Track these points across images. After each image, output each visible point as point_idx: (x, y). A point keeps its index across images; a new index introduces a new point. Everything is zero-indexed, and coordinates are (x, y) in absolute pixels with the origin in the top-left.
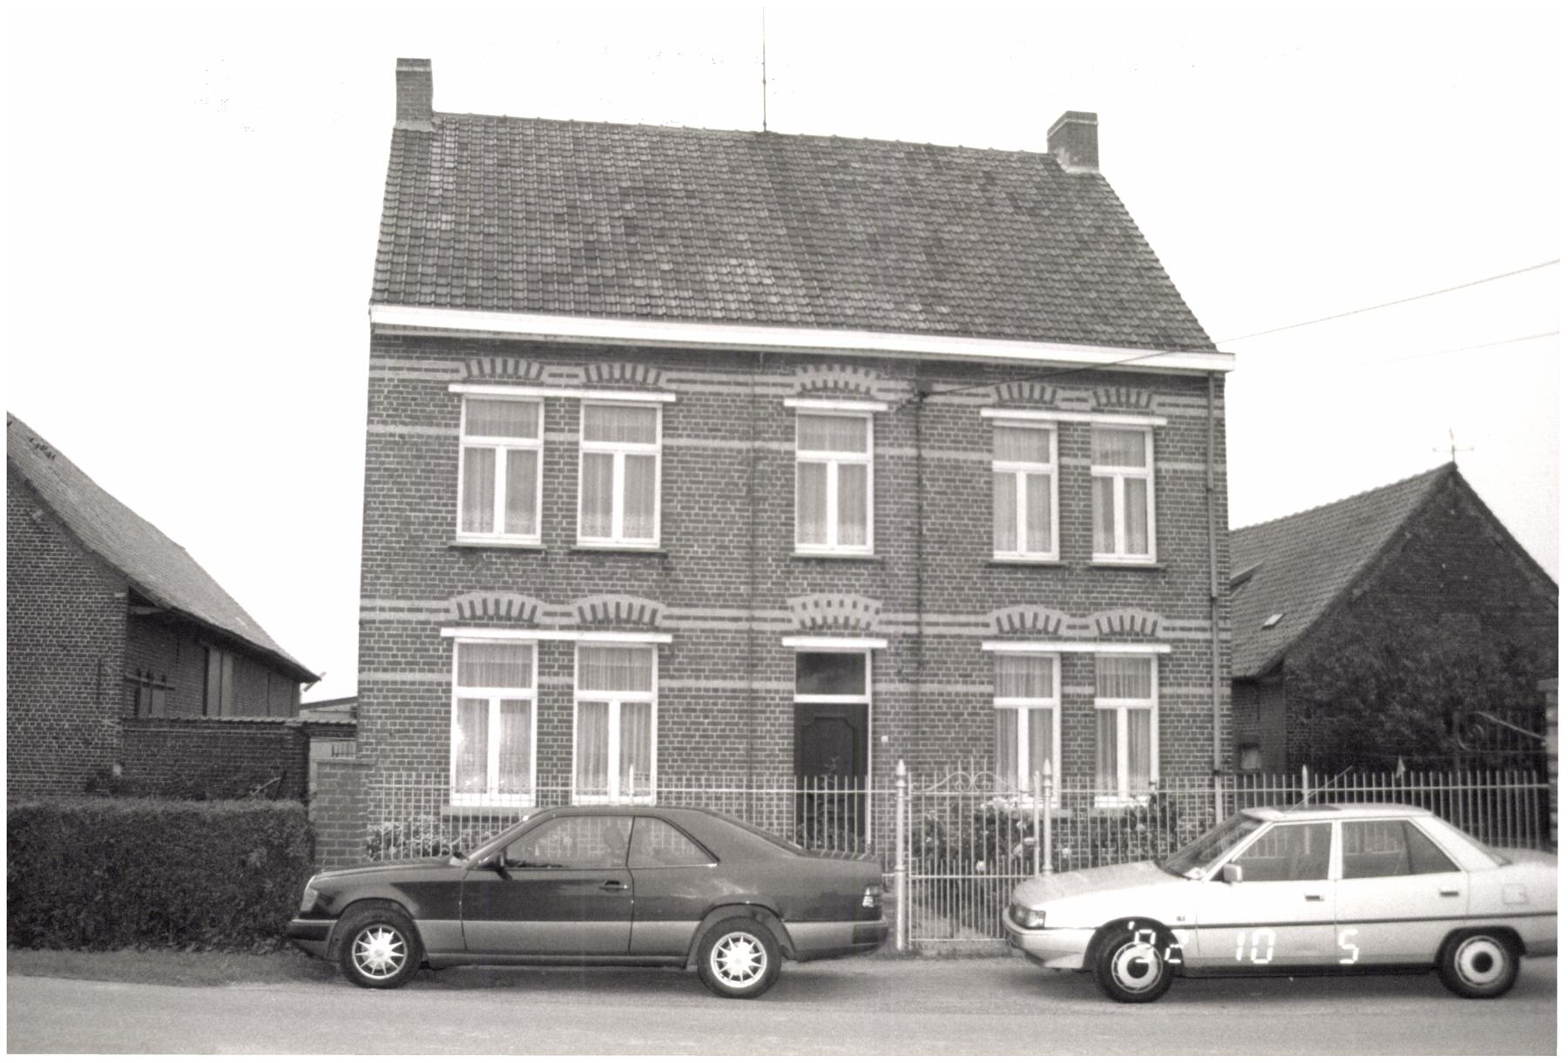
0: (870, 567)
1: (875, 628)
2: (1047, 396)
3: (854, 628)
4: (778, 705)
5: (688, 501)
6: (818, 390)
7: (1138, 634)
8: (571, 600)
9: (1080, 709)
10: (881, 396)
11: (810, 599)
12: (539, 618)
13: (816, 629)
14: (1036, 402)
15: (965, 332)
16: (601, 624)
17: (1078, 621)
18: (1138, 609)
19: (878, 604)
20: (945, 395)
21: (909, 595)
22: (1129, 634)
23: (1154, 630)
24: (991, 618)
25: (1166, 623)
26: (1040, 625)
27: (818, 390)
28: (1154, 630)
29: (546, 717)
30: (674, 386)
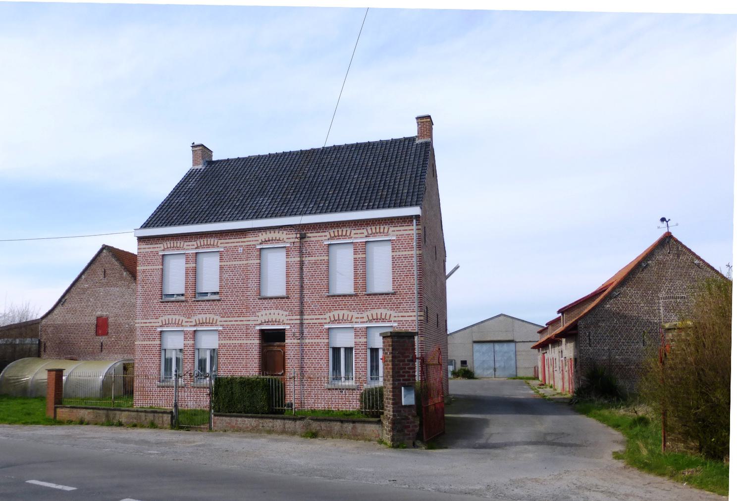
0: (204, 302)
1: (286, 322)
2: (348, 234)
3: (279, 322)
4: (253, 348)
5: (238, 281)
6: (267, 241)
7: (383, 319)
8: (193, 317)
9: (360, 347)
10: (287, 241)
11: (264, 312)
12: (184, 324)
13: (267, 322)
14: (344, 236)
15: (400, 205)
16: (377, 320)
17: (360, 316)
18: (384, 310)
19: (287, 313)
20: (313, 236)
21: (297, 309)
22: (380, 319)
23: (216, 322)
24: (327, 316)
25: (396, 315)
26: (345, 318)
27: (267, 241)
28: (216, 322)
29: (357, 352)
30: (222, 245)
